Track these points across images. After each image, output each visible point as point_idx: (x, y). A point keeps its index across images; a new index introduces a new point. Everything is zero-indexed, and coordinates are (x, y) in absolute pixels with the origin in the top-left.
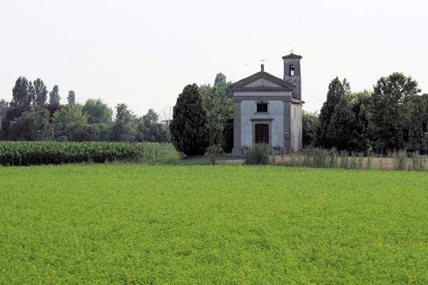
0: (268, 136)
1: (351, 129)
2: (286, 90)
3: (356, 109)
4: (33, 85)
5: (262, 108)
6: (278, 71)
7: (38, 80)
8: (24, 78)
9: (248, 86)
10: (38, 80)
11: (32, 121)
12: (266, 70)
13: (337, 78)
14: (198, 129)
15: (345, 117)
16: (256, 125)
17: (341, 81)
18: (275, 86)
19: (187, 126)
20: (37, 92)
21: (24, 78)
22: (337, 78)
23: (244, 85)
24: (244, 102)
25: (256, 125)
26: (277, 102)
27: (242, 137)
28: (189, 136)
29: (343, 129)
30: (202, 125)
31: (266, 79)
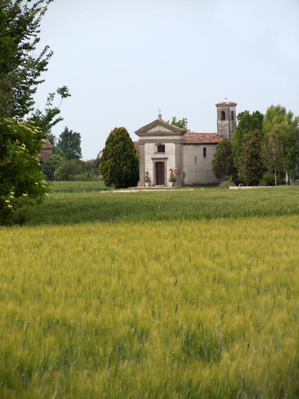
0: (164, 172)
18: (169, 131)
23: (148, 130)
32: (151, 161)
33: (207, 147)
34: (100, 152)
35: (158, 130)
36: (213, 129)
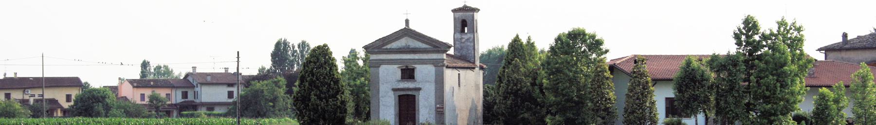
0: (414, 110)
1: (523, 102)
2: (438, 52)
3: (598, 79)
4: (296, 48)
5: (408, 74)
6: (443, 31)
7: (304, 43)
8: (285, 40)
9: (389, 46)
10: (304, 43)
11: (262, 91)
12: (412, 26)
13: (517, 36)
14: (327, 101)
15: (516, 85)
16: (399, 96)
17: (524, 41)
18: (424, 46)
19: (313, 97)
20: (302, 56)
21: (285, 40)
22: (517, 36)
23: (387, 44)
24: (383, 69)
25: (399, 96)
26: (425, 66)
27: (381, 112)
28: (315, 110)
29: (513, 100)
30: (334, 96)
31: (411, 37)
32: (391, 93)
33: (462, 72)
34: (74, 82)
35: (404, 44)
36: (138, 77)
